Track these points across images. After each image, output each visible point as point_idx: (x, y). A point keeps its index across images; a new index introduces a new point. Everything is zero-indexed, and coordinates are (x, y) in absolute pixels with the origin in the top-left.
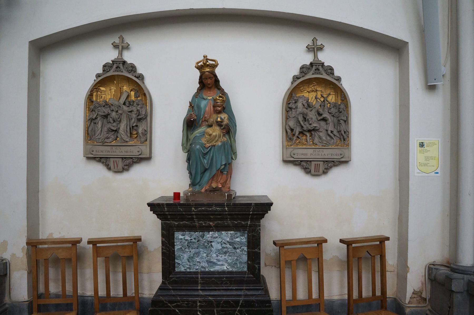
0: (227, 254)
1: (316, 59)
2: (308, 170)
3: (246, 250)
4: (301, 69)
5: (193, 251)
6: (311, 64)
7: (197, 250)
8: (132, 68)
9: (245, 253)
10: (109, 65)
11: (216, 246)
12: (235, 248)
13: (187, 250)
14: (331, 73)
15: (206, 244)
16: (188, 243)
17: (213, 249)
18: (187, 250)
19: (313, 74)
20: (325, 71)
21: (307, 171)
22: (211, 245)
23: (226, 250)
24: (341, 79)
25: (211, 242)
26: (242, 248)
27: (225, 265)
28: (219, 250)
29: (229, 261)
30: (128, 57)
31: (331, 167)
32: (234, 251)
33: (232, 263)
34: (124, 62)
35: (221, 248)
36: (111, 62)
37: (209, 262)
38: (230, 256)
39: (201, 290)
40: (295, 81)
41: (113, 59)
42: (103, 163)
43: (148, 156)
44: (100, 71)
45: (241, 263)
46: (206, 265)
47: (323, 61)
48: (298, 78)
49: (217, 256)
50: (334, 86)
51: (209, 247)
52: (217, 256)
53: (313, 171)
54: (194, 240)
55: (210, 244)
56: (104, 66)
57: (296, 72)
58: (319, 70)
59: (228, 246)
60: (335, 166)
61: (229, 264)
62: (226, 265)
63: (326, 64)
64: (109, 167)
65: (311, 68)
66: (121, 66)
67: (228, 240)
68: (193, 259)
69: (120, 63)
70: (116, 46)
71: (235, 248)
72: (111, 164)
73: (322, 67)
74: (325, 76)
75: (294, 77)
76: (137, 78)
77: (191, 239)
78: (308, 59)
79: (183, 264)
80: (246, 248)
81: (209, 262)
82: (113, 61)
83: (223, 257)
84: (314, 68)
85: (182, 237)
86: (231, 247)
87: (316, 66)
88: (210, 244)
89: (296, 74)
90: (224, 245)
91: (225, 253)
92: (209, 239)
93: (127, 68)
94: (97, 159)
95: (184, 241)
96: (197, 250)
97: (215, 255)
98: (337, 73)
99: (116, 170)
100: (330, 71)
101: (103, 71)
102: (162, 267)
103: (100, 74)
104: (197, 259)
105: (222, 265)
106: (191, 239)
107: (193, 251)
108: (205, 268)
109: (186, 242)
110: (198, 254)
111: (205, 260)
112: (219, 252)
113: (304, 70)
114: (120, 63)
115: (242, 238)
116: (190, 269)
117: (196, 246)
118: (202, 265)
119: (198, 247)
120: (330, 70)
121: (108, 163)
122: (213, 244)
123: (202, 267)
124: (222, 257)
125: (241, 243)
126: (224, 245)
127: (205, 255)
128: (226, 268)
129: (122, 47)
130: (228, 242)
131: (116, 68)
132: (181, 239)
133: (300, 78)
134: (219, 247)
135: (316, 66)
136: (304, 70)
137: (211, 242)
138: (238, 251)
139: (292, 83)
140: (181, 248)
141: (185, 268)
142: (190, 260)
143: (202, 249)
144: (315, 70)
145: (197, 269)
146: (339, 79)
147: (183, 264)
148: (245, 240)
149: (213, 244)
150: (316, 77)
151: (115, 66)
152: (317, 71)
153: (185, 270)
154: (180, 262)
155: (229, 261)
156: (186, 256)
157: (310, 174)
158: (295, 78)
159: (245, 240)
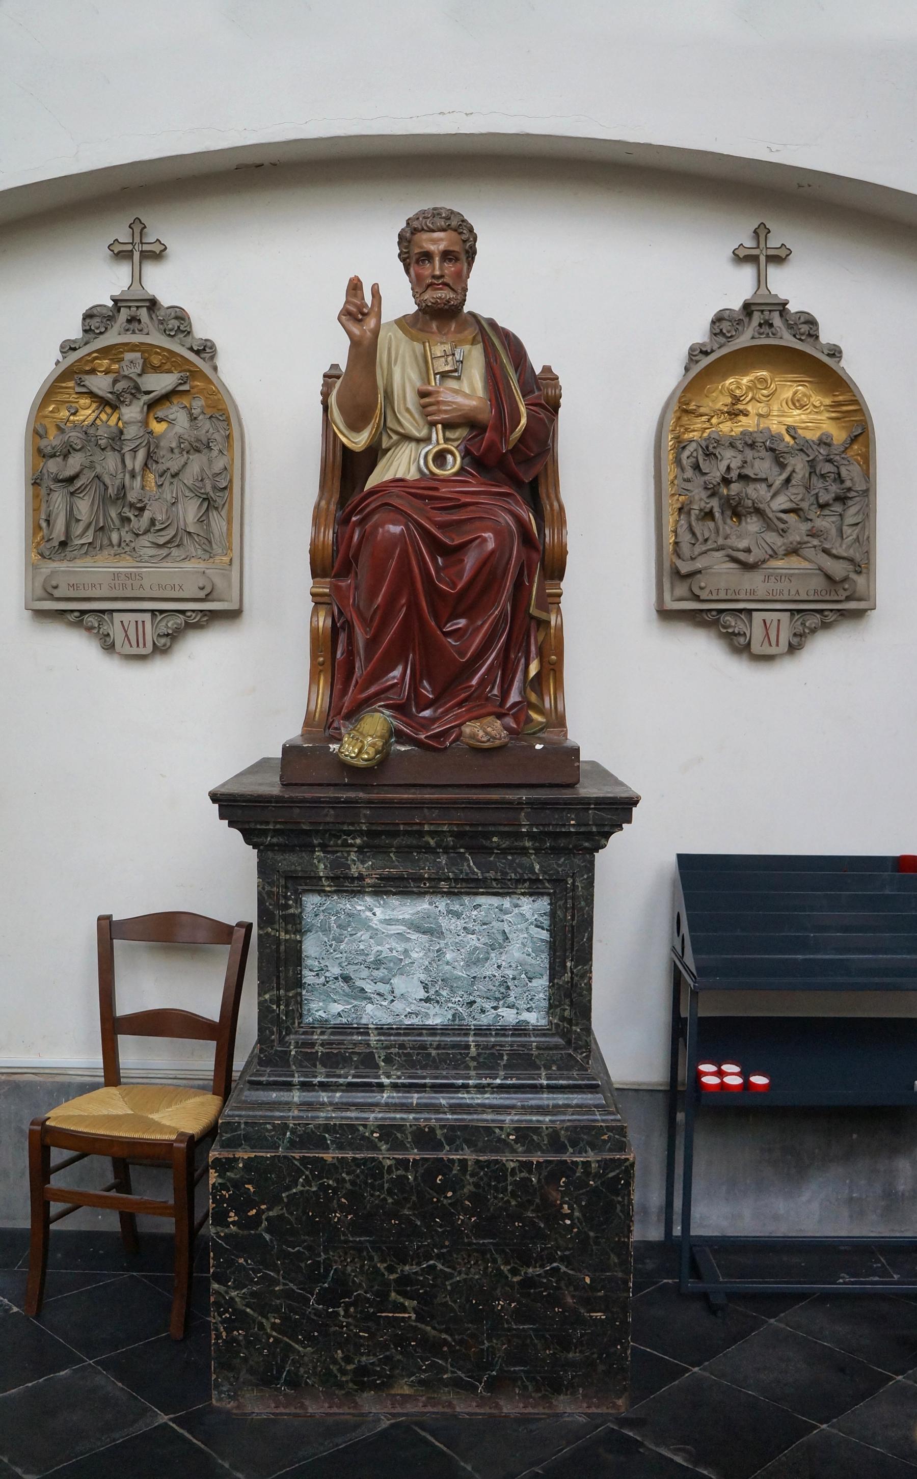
0: (371, 958)
1: (763, 290)
2: (742, 640)
3: (305, 972)
4: (713, 322)
5: (489, 970)
6: (748, 308)
7: (475, 971)
8: (179, 323)
9: (309, 962)
10: (104, 311)
11: (409, 987)
12: (346, 979)
13: (510, 973)
14: (810, 335)
15: (444, 993)
16: (505, 996)
17: (423, 977)
18: (510, 973)
19: (753, 338)
20: (790, 327)
21: (740, 646)
22: (426, 988)
23: (376, 973)
24: (840, 352)
25: (428, 1000)
26: (322, 979)
27: (381, 922)
28: (401, 972)
29: (366, 936)
30: (165, 284)
31: (813, 631)
32: (350, 970)
33: (357, 930)
34: (153, 304)
35: (395, 981)
36: (110, 304)
37: (434, 932)
38: (362, 952)
39: (395, 1086)
40: (697, 362)
41: (117, 293)
42: (89, 629)
43: (235, 606)
44: (75, 332)
45: (325, 930)
46: (444, 922)
47: (783, 296)
48: (706, 353)
49: (406, 951)
50: (822, 370)
51: (434, 982)
52: (406, 951)
53: (756, 648)
54: (488, 1005)
55: (432, 992)
56: (88, 316)
57: (699, 333)
58: (771, 325)
59: (369, 988)
60: (826, 626)
61: (365, 925)
62: (375, 922)
63: (792, 308)
64: (109, 641)
65: (746, 320)
66: (143, 314)
67: (369, 1008)
68: (489, 941)
69: (138, 308)
70: (121, 255)
71: (346, 979)
72: (118, 635)
73: (781, 315)
74: (788, 340)
75: (692, 349)
76: (197, 352)
77: (495, 1008)
78: (736, 288)
79: (522, 921)
80: (309, 977)
81: (434, 932)
82: (116, 301)
83: (384, 948)
84: (757, 318)
85: (526, 1016)
86: (359, 983)
87: (761, 310)
88: (432, 992)
89: (699, 340)
90: (383, 988)
91: (378, 963)
92: (433, 1009)
93: (161, 322)
94: (72, 617)
95: (521, 1004)
96: (475, 971)
97: (414, 955)
98: (826, 336)
99: (128, 650)
100: (805, 328)
101: (85, 331)
102: (684, 894)
103: (74, 341)
104: (475, 943)
105: (388, 922)
106: (495, 1008)
107: (489, 970)
108: (450, 912)
109: (512, 999)
110: (473, 961)
111: (450, 939)
112: (399, 967)
113: (725, 326)
114: (138, 308)
115: (321, 1013)
116: (501, 909)
117: (480, 986)
118: (460, 923)
119: (473, 984)
120: (807, 326)
121: (105, 629)
122: (422, 994)
123: (458, 915)
124: (391, 950)
125: (328, 998)
126: (383, 988)
127: (449, 956)
128: (378, 911)
129: (143, 253)
130: (370, 1000)
131: (129, 321)
132: (528, 1010)
133: (712, 351)
134: (399, 983)
135: (761, 310)
136: (725, 326)
137: (428, 1000)
138: (336, 971)
139: (687, 369)
140: (530, 979)
141: (516, 910)
142: (500, 938)
143: (458, 978)
144: (760, 325)
145: (477, 907)
146: (835, 353)
147: (522, 921)
148: (313, 1006)
149: (422, 994)
150: (765, 340)
151: (124, 314)
152: (766, 329)
153: (517, 906)
154: (534, 930)
155: (366, 936)
156: (516, 952)
157: (745, 656)
158: (697, 353)
159: (313, 1006)
